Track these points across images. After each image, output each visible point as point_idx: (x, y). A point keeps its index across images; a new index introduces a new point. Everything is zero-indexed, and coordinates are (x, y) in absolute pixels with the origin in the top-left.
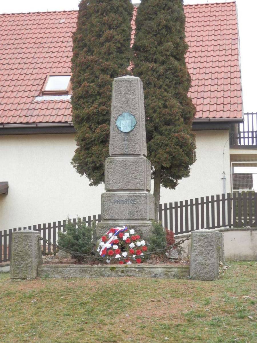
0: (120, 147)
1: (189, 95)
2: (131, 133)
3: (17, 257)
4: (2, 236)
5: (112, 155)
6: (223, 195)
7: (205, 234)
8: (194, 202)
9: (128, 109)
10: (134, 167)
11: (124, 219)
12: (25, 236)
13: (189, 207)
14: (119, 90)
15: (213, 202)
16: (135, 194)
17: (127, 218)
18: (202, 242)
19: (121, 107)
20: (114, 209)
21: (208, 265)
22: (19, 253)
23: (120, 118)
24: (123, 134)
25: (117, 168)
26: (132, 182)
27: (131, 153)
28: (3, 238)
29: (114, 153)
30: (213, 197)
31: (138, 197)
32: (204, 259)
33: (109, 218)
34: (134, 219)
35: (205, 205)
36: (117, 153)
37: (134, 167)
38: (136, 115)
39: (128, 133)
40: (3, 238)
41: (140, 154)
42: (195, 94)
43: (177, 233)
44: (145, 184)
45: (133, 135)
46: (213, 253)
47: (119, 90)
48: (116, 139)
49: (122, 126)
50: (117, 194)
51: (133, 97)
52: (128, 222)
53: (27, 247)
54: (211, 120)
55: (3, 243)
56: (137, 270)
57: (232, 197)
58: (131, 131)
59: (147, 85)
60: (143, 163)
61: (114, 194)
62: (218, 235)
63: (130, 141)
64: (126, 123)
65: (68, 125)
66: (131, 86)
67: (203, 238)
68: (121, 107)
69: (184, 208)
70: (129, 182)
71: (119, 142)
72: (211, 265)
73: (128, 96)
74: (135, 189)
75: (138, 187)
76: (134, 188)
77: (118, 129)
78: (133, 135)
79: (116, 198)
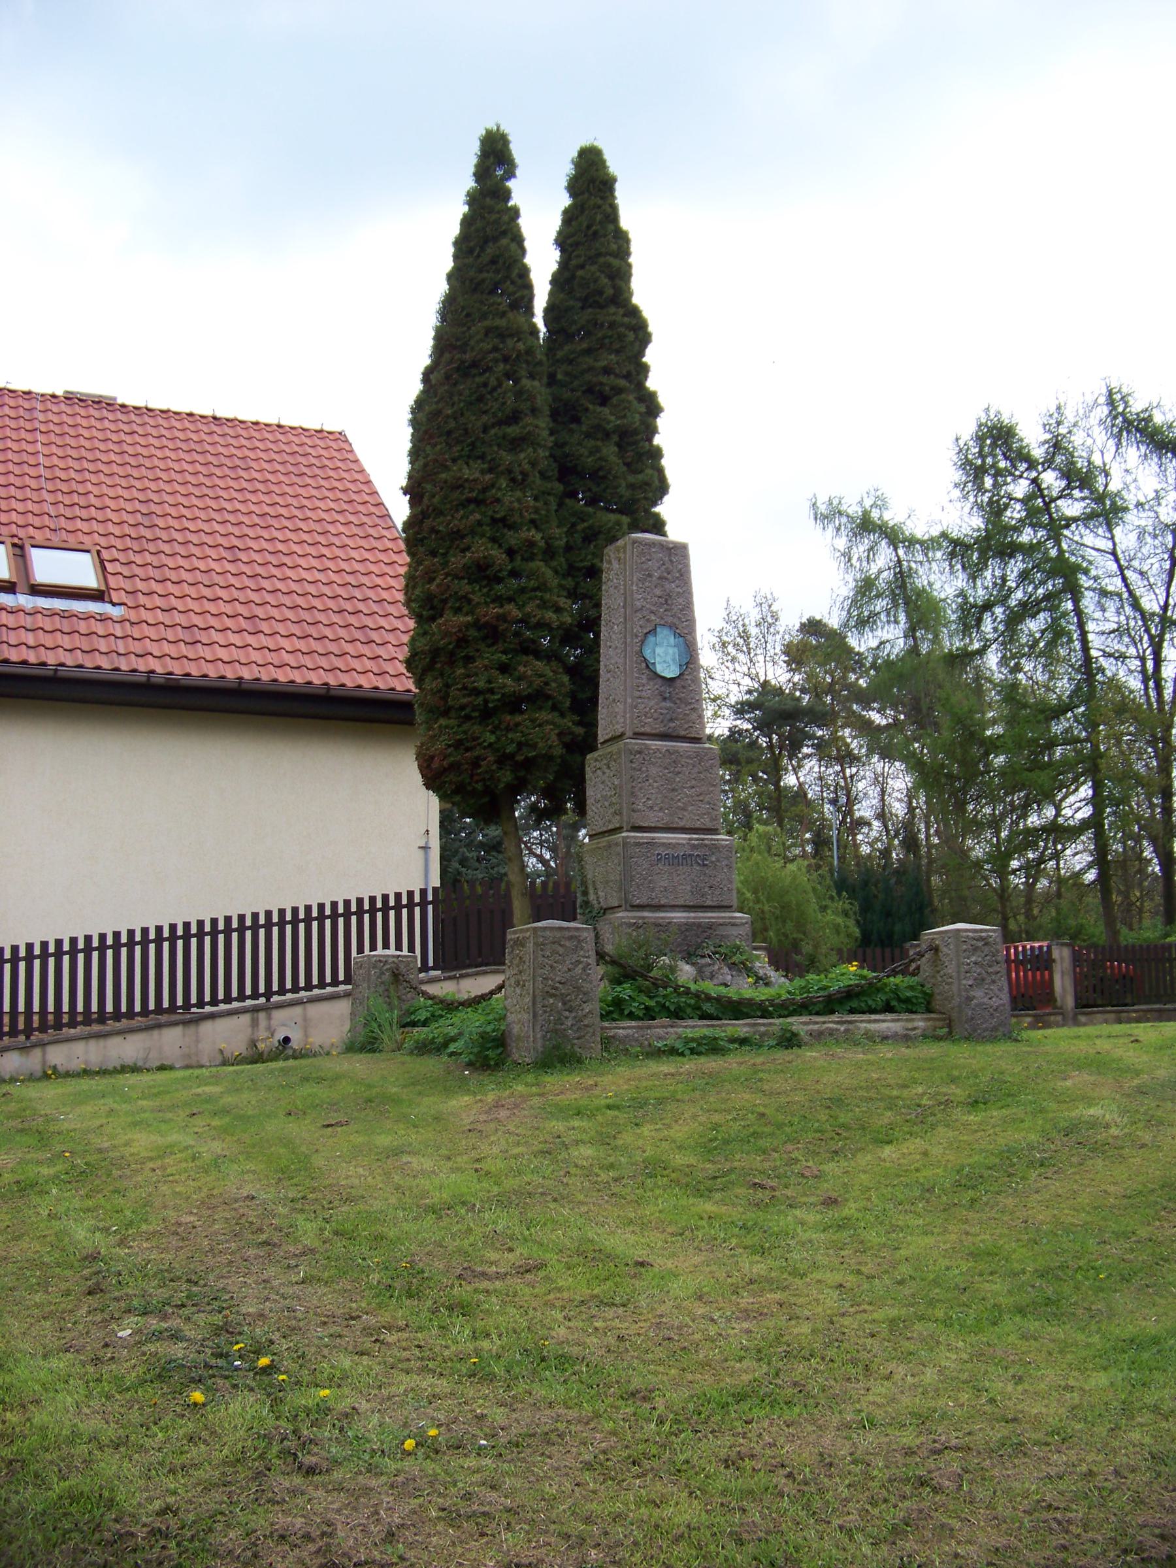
0: (655, 715)
1: (412, 624)
2: (678, 681)
3: (551, 1001)
5: (635, 734)
6: (423, 892)
8: (235, 925)
9: (670, 620)
10: (696, 770)
12: (571, 938)
13: (262, 932)
14: (645, 566)
17: (688, 903)
18: (979, 953)
20: (655, 877)
21: (996, 1010)
22: (556, 989)
23: (651, 639)
24: (660, 681)
25: (654, 770)
26: (690, 808)
27: (683, 733)
29: (643, 730)
33: (643, 900)
35: (367, 917)
36: (647, 729)
37: (696, 770)
39: (672, 679)
42: (398, 624)
43: (201, 1003)
45: (684, 687)
47: (645, 566)
48: (644, 694)
49: (658, 659)
50: (659, 838)
51: (679, 589)
52: (692, 915)
53: (579, 970)
55: (7, 1008)
56: (842, 1029)
57: (430, 898)
61: (653, 839)
64: (667, 654)
65: (51, 673)
67: (980, 944)
68: (652, 612)
69: (208, 939)
70: (684, 809)
71: (652, 703)
73: (667, 586)
76: (698, 825)
77: (647, 666)
78: (684, 687)
79: (660, 850)
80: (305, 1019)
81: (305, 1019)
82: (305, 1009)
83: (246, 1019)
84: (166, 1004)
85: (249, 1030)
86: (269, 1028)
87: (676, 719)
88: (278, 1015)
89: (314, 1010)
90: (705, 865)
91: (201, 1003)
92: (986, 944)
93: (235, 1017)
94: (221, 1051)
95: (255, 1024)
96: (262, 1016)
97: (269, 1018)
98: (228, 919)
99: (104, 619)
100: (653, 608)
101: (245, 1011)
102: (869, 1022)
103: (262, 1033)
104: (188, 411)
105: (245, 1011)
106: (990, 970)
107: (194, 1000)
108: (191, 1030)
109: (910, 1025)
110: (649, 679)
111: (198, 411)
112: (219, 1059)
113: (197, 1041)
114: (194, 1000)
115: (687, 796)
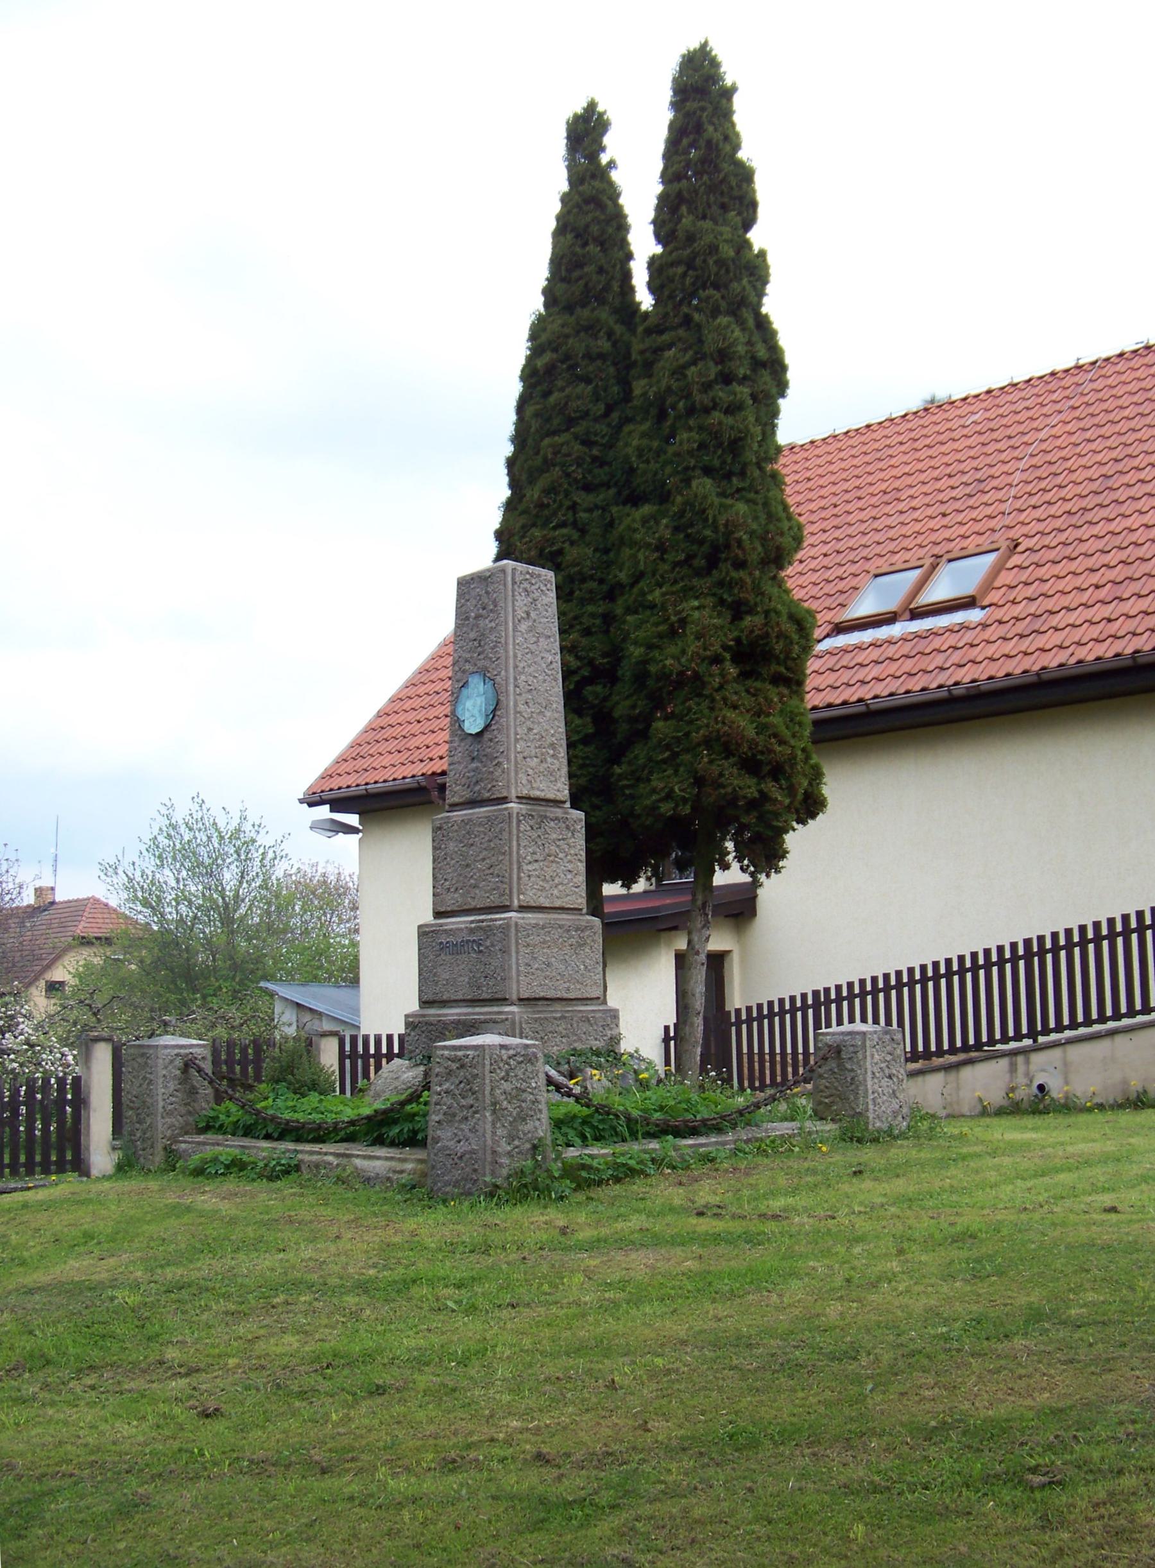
0: (464, 781)
2: (487, 736)
4: (732, 1024)
7: (460, 1053)
11: (461, 1001)
15: (1083, 943)
16: (482, 921)
18: (453, 1079)
19: (467, 661)
21: (461, 1158)
23: (465, 692)
27: (487, 795)
28: (734, 1029)
30: (1083, 929)
31: (488, 931)
32: (456, 1135)
34: (479, 1000)
38: (498, 679)
39: (480, 734)
40: (734, 1029)
41: (506, 798)
43: (992, 1041)
44: (515, 890)
45: (491, 740)
46: (477, 1116)
50: (446, 924)
51: (493, 624)
52: (470, 1010)
54: (872, 707)
58: (487, 727)
59: (564, 594)
60: (505, 826)
62: (853, 1039)
63: (484, 759)
65: (1035, 679)
66: (487, 593)
67: (454, 1066)
68: (467, 661)
70: (475, 887)
72: (467, 1156)
74: (490, 908)
75: (494, 899)
76: (487, 903)
78: (491, 740)
80: (1066, 1064)
81: (1066, 1064)
82: (1065, 1052)
83: (1004, 1063)
84: (971, 1041)
85: (1008, 1076)
86: (1027, 1074)
87: (481, 780)
88: (1037, 1058)
89: (1076, 1053)
90: (481, 952)
91: (992, 1041)
92: (462, 1066)
93: (994, 1061)
94: (980, 1100)
95: (1013, 1069)
96: (1020, 1059)
97: (1027, 1062)
98: (1000, 949)
99: (964, 627)
100: (468, 656)
101: (1004, 1054)
102: (365, 1157)
103: (1021, 1079)
104: (985, 389)
105: (1004, 1054)
106: (463, 1102)
107: (984, 1039)
108: (952, 1076)
109: (398, 1166)
110: (462, 740)
111: (1060, 366)
112: (979, 1108)
113: (958, 1088)
114: (984, 1039)
115: (480, 870)
